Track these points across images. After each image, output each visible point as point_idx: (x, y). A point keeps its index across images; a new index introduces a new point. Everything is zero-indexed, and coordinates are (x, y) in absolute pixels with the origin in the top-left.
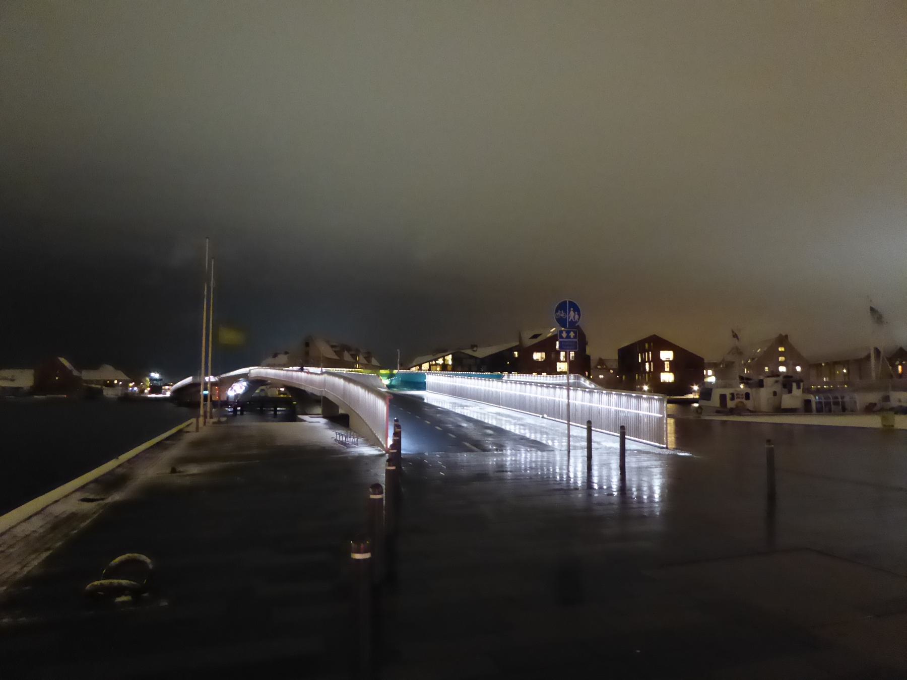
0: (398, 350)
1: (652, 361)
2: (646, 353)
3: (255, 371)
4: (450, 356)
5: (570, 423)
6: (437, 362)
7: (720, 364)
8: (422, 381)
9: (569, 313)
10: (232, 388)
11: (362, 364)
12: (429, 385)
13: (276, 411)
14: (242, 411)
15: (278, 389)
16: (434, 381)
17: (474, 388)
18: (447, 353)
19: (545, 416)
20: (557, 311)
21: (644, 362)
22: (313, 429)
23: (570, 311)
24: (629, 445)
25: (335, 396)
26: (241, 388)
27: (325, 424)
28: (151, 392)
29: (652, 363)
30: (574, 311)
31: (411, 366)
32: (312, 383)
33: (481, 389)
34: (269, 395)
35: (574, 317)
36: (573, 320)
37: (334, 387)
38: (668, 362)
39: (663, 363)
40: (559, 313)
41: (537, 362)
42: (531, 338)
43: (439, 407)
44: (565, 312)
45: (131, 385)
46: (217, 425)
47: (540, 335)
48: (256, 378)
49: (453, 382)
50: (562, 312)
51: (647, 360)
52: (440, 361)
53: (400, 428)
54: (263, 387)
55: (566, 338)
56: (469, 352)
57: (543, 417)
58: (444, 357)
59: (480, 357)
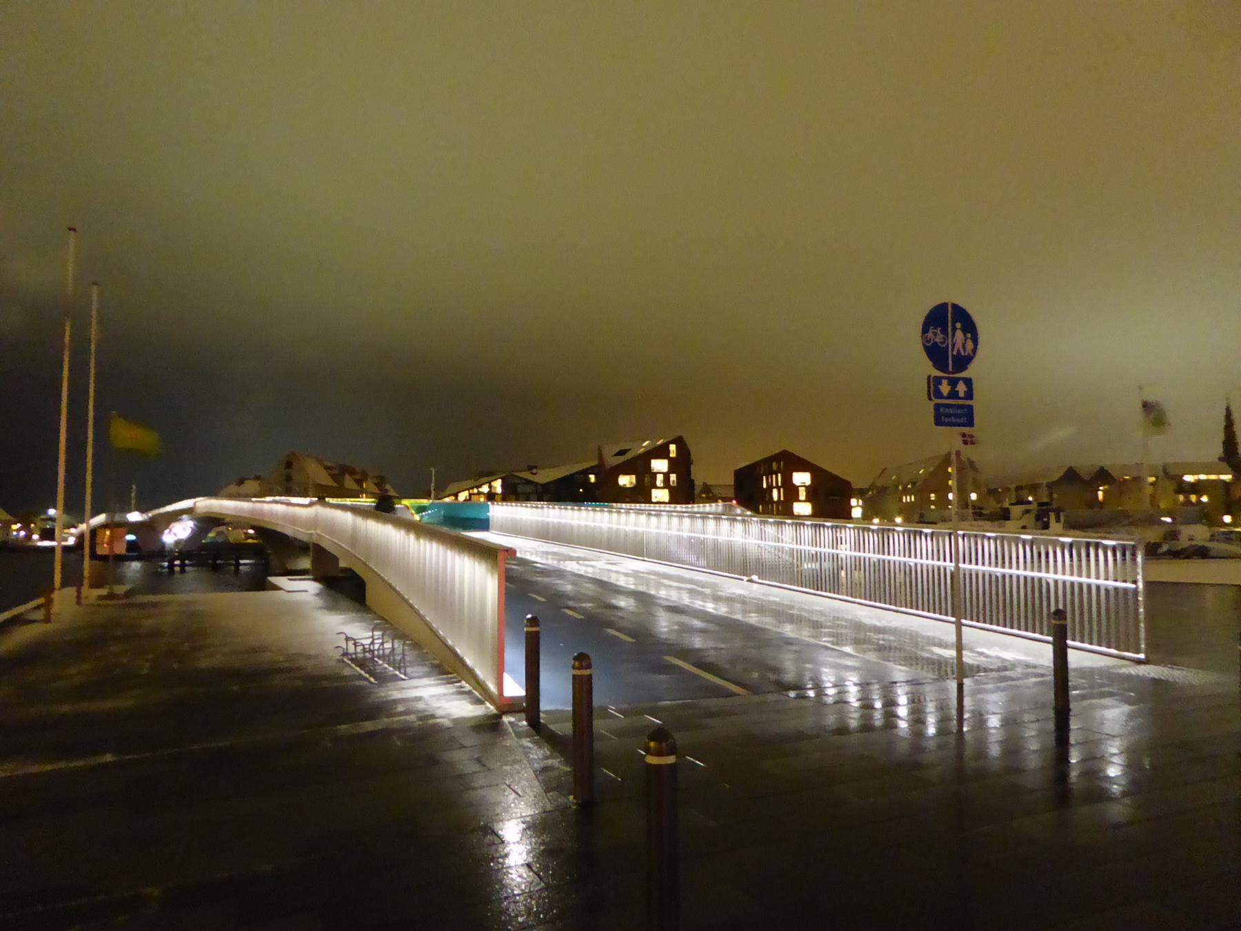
0: (433, 470)
1: (782, 486)
2: (774, 476)
3: (203, 504)
4: (499, 481)
5: (963, 621)
6: (480, 490)
7: (868, 490)
8: (482, 516)
9: (953, 336)
10: (171, 530)
11: (371, 493)
12: (495, 521)
13: (238, 564)
14: (183, 566)
15: (245, 531)
16: (505, 515)
17: (586, 526)
18: (494, 478)
19: (755, 578)
20: (925, 330)
21: (770, 488)
22: (293, 611)
23: (954, 329)
24: (1076, 659)
25: (337, 544)
26: (184, 529)
27: (317, 595)
28: (42, 538)
29: (782, 490)
30: (965, 331)
31: (443, 496)
32: (293, 520)
33: (601, 528)
34: (231, 539)
35: (964, 345)
36: (963, 354)
37: (332, 528)
38: (804, 488)
39: (796, 488)
40: (930, 335)
41: (624, 489)
42: (616, 455)
43: (537, 563)
44: (945, 332)
45: (14, 527)
46: (109, 602)
47: (629, 450)
48: (207, 515)
49: (543, 516)
50: (939, 332)
51: (774, 485)
52: (485, 489)
53: (589, 667)
54: (222, 528)
55: (949, 397)
56: (526, 475)
57: (751, 581)
58: (490, 483)
59: (542, 482)
